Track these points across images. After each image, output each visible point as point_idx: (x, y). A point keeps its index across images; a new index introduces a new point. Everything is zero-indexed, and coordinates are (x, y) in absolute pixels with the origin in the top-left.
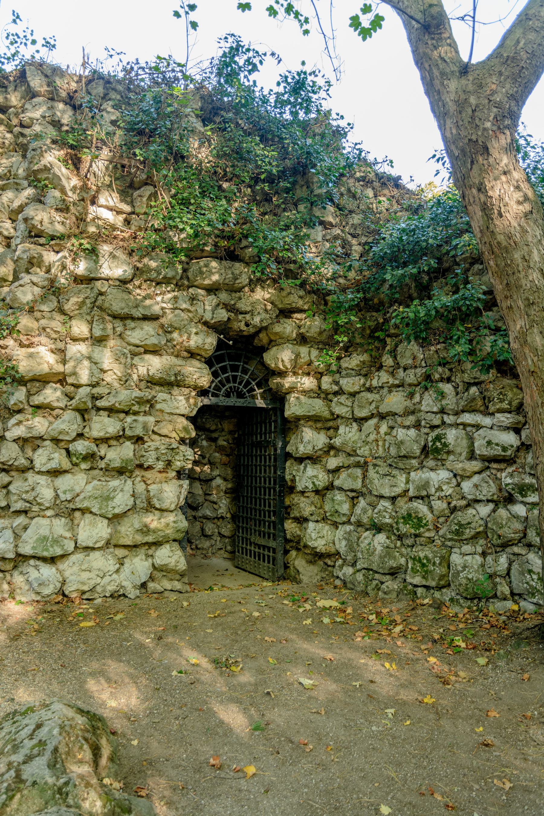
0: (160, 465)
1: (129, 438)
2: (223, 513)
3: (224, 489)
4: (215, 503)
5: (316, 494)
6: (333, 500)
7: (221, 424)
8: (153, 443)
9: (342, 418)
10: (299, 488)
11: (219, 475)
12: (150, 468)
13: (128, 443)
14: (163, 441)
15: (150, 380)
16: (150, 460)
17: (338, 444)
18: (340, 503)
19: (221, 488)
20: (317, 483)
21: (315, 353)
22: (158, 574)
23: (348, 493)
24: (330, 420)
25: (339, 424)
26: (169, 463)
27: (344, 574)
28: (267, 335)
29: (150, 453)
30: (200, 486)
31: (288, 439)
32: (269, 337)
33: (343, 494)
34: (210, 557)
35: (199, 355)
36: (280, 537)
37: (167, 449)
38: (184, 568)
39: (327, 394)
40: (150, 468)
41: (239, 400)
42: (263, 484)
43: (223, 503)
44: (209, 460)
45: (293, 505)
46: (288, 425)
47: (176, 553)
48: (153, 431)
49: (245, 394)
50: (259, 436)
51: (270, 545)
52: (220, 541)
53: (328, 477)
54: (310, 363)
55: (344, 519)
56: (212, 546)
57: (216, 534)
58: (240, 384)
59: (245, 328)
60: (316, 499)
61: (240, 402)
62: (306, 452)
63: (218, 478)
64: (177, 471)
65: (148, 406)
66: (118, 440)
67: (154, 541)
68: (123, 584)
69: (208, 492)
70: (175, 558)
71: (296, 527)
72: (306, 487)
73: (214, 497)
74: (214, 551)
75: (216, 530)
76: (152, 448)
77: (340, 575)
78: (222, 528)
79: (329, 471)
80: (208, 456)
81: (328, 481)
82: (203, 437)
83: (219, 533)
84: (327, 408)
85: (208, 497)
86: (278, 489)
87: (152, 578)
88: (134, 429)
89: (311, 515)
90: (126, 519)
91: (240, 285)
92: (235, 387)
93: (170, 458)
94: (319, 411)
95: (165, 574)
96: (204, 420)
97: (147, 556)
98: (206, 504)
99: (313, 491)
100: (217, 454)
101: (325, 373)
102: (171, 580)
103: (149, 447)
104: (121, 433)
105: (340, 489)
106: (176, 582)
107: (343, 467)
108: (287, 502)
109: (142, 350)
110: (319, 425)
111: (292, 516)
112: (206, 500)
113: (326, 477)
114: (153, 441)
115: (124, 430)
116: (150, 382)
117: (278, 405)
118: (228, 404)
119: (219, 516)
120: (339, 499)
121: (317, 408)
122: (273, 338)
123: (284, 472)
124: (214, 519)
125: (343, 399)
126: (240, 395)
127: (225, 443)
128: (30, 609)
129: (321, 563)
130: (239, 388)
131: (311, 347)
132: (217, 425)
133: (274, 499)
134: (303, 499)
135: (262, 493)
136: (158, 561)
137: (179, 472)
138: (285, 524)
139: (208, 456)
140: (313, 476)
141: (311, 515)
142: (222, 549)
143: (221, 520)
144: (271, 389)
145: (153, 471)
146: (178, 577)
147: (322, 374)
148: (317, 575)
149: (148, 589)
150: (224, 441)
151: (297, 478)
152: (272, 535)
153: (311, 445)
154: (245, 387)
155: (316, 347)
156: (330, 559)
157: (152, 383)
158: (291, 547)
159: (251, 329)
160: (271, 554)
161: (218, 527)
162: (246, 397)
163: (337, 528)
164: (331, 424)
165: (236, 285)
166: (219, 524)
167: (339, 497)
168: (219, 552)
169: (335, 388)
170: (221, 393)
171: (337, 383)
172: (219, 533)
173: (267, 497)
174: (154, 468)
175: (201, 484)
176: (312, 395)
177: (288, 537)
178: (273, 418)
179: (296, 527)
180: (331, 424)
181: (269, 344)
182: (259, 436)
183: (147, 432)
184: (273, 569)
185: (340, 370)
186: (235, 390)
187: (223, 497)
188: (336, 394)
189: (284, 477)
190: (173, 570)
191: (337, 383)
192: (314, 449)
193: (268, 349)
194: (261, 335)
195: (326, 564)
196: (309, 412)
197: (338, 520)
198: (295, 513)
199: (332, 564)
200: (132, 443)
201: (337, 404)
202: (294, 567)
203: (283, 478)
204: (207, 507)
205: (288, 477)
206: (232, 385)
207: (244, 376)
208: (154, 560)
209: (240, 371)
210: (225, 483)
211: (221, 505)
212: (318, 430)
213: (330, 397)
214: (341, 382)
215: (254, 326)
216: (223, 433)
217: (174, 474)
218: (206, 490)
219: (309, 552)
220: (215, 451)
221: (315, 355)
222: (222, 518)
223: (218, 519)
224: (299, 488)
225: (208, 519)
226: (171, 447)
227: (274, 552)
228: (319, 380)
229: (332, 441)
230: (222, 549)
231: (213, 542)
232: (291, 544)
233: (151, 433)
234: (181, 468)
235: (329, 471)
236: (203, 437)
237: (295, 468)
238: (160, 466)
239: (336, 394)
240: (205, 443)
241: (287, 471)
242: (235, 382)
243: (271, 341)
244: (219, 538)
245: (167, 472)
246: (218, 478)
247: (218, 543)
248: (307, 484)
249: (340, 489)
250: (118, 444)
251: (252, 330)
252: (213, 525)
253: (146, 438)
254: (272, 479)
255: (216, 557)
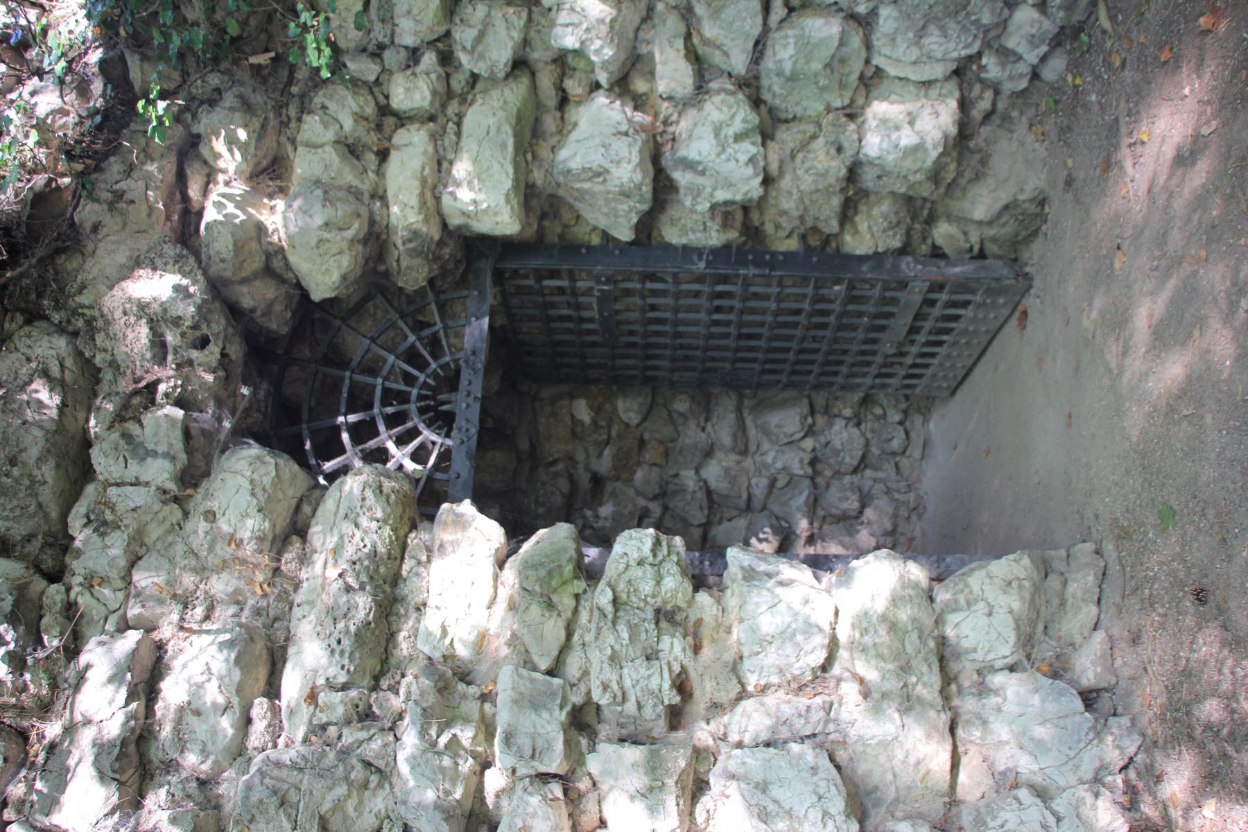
0: (674, 647)
1: (575, 757)
2: (801, 461)
3: (734, 457)
4: (773, 482)
5: (772, 139)
6: (793, 78)
7: (554, 462)
8: (594, 671)
9: (526, 42)
10: (754, 188)
11: (697, 471)
12: (682, 686)
13: (594, 764)
14: (589, 637)
15: (367, 681)
16: (654, 683)
17: (608, 52)
18: (806, 48)
19: (731, 464)
20: (738, 126)
21: (312, 127)
22: (1046, 650)
23: (774, 18)
24: (534, 87)
25: (548, 56)
26: (666, 616)
27: (1033, 41)
28: (245, 281)
29: (628, 683)
30: (725, 525)
31: (596, 240)
32: (256, 276)
33: (775, 35)
34: (919, 497)
35: (298, 508)
36: (896, 267)
37: (614, 623)
38: (1026, 561)
39: (450, 94)
40: (682, 686)
41: (464, 382)
42: (732, 317)
43: (775, 459)
44: (655, 498)
45: (801, 218)
46: (552, 237)
47: (976, 589)
48: (551, 673)
49: (445, 367)
50: (586, 326)
51: (918, 299)
52: (876, 469)
53: (718, 92)
54: (352, 150)
55: (856, 41)
56: (888, 491)
57: (856, 479)
58: (409, 379)
59: (214, 350)
60: (787, 137)
61: (472, 384)
62: (635, 158)
63: (704, 474)
64: (696, 589)
65: (461, 687)
66: (581, 796)
67: (936, 666)
68: (1089, 776)
69: (742, 502)
70: (992, 593)
71: (869, 216)
72: (752, 160)
73: (760, 486)
74: (903, 485)
75: (847, 479)
76: (611, 676)
77: (1032, 57)
78: (842, 463)
79: (701, 88)
80: (642, 502)
81: (733, 93)
82: (589, 513)
83: (856, 470)
84: (495, 94)
85: (757, 503)
86: (753, 271)
87: (1057, 671)
88: (540, 743)
89: (839, 150)
90: (862, 768)
91: (69, 363)
92: (421, 398)
93: (650, 614)
94: (501, 114)
95: (1040, 627)
96: (541, 510)
97: (983, 690)
98: (776, 509)
99: (764, 145)
100: (639, 475)
101: (381, 99)
102: (1063, 603)
103: (605, 687)
104: (556, 789)
105: (759, 47)
106: (1073, 587)
107: (688, 37)
108: (792, 244)
109: (260, 707)
110: (550, 122)
111: (834, 226)
112: (764, 508)
113: (717, 99)
114: (586, 673)
115: (544, 778)
116: (376, 679)
117: (486, 269)
118: (476, 418)
119: (809, 471)
120: (791, 50)
121: (492, 121)
122: (257, 263)
123: (699, 251)
124: (815, 486)
125: (464, 35)
126: (451, 381)
127: (607, 452)
128: (101, 50)
129: (985, 131)
130: (425, 385)
131: (293, 142)
132: (556, 474)
133: (780, 284)
134: (786, 183)
135: (758, 318)
136: (1005, 650)
137: (699, 583)
138: (858, 252)
139: (642, 502)
140: (717, 136)
141: (839, 150)
142: (897, 465)
143: (819, 466)
144: (431, 282)
145: (693, 675)
146: (1054, 582)
147: (384, 110)
148: (1022, 144)
149: (1103, 685)
150: (600, 455)
151: (721, 195)
152: (888, 294)
153: (612, 140)
154: (422, 365)
155: (293, 124)
156: (972, 103)
157: (383, 673)
158: (924, 239)
159: (216, 328)
160: (944, 297)
161: (838, 474)
162: (456, 361)
163: (879, 71)
164: (546, 81)
165: (68, 376)
166: (828, 473)
167: (783, 53)
168: (906, 472)
169: (429, 59)
170: (439, 440)
171: (414, 55)
172: (856, 470)
173: (773, 306)
174: (684, 670)
175: (720, 522)
176: (450, 137)
177: (897, 243)
178: (530, 282)
179: (869, 216)
180: (546, 81)
181: (282, 280)
182: (586, 326)
183: (554, 694)
184: (989, 292)
185: (371, 48)
186: (433, 398)
187: (758, 459)
188: (446, 59)
189: (714, 251)
190: (1032, 601)
191: (414, 55)
192: (626, 134)
193: (299, 285)
194: (247, 302)
195: (988, 116)
196: (503, 145)
197: (856, 67)
198: (827, 213)
199: (989, 95)
200: (592, 749)
201: (482, 57)
202: (990, 223)
203: (720, 254)
204: (784, 504)
205: (715, 238)
206: (413, 407)
207: (387, 368)
208: (999, 664)
209: (370, 380)
210: (719, 454)
211: (779, 465)
212: (564, 130)
213: (459, 81)
214: (409, 41)
215: (203, 312)
216: (580, 457)
217: (703, 598)
218: (736, 508)
219: (953, 166)
220: (629, 481)
221: (319, 128)
222: (813, 462)
223: (816, 473)
224: (754, 188)
225: (816, 500)
226: (609, 609)
227: (940, 287)
228: (402, 119)
229: (603, 78)
230: (897, 465)
231: (879, 487)
232: (916, 237)
233: (557, 681)
234: (684, 573)
235: (701, 88)
236: (589, 513)
237: (688, 202)
238: (677, 649)
239: (446, 59)
240: (606, 510)
241: (695, 238)
242: (403, 398)
243: (268, 271)
244: (868, 472)
245: (699, 622)
246: (704, 474)
247: (880, 475)
248: (743, 158)
249: (759, 47)
250: (593, 796)
251: (218, 325)
252: (833, 490)
253: (576, 698)
254: (720, 288)
255: (919, 480)
